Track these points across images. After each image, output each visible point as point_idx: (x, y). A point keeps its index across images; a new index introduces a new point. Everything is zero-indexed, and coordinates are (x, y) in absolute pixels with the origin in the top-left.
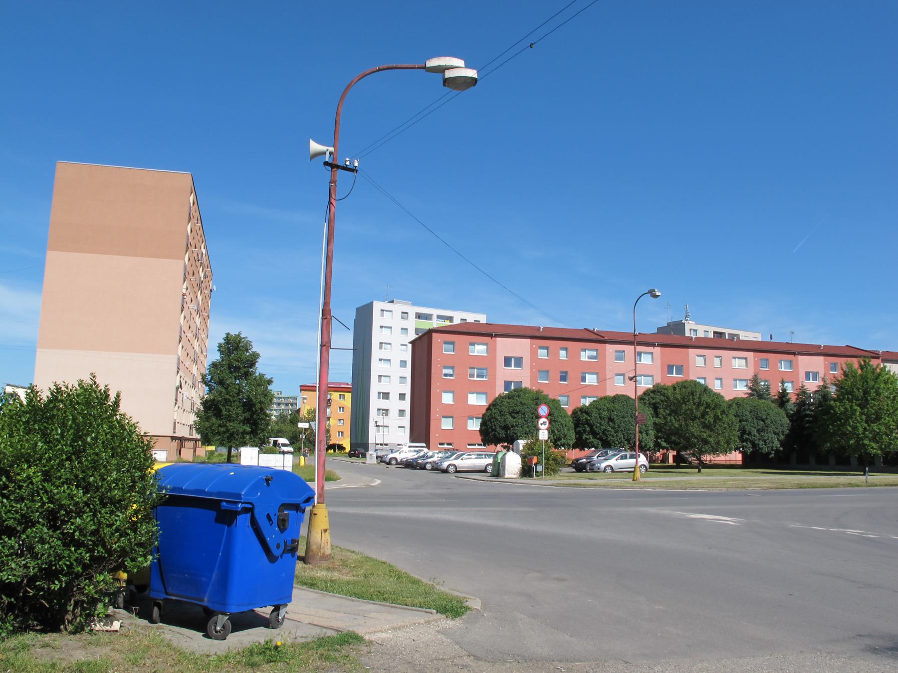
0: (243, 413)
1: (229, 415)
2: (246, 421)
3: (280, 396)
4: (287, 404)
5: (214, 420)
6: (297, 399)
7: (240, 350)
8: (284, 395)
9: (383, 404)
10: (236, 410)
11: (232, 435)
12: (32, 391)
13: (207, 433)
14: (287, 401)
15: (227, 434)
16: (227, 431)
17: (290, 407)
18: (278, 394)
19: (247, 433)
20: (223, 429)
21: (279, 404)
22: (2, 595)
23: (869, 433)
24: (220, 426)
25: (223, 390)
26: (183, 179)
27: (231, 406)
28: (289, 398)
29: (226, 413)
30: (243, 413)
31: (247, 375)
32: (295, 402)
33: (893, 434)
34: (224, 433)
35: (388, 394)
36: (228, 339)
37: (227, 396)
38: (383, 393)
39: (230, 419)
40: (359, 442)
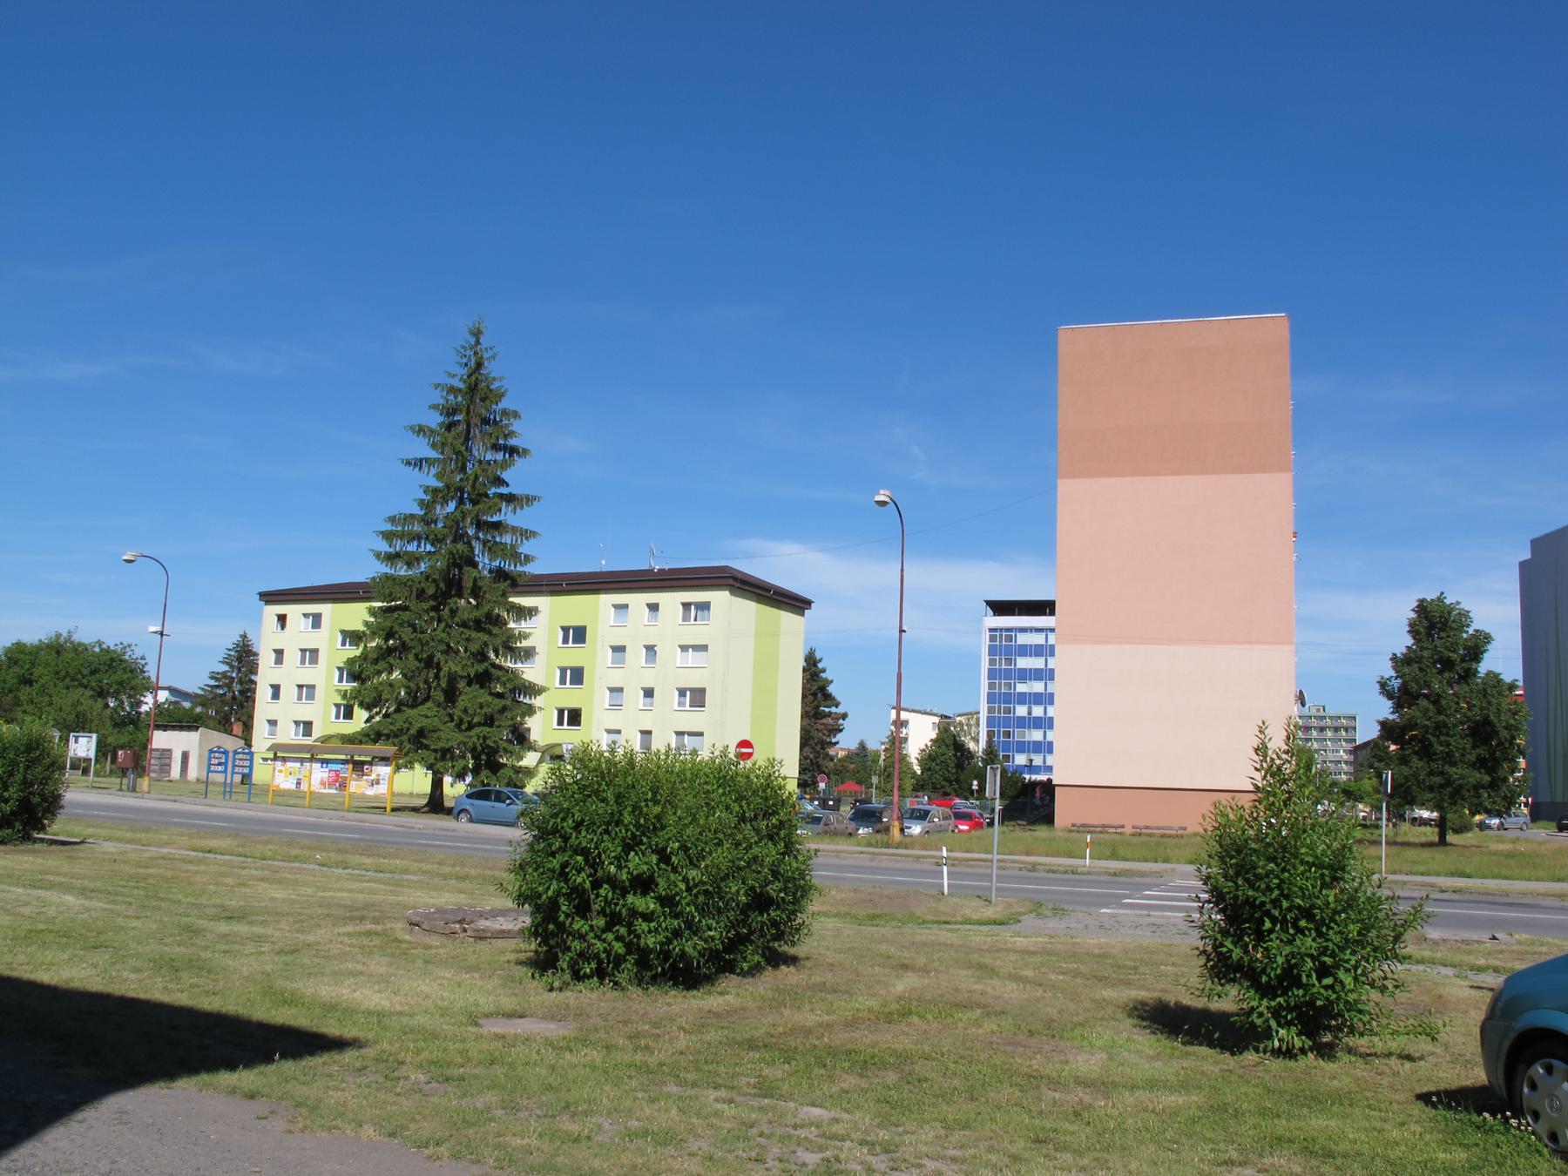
0: (1474, 748)
1: (1448, 754)
2: (1481, 764)
3: (1322, 713)
4: (1336, 729)
5: (1416, 762)
6: (1355, 718)
7: (1451, 628)
8: (1330, 711)
9: (308, 675)
10: (1459, 742)
11: (1458, 790)
12: (824, 671)
13: (1409, 787)
14: (1337, 724)
15: (1450, 789)
16: (1448, 782)
17: (1344, 733)
18: (1318, 710)
19: (1483, 787)
20: (1438, 780)
21: (1322, 729)
22: (511, 599)
23: (390, 673)
24: (1431, 773)
25: (1431, 707)
26: (1272, 327)
27: (1448, 735)
28: (1340, 718)
29: (1441, 748)
30: (1474, 748)
31: (1468, 675)
32: (1351, 724)
33: (1454, 756)
34: (1442, 786)
35: (702, 691)
36: (1422, 608)
37: (1441, 718)
38: (693, 690)
39: (1449, 758)
40: (1559, 798)
